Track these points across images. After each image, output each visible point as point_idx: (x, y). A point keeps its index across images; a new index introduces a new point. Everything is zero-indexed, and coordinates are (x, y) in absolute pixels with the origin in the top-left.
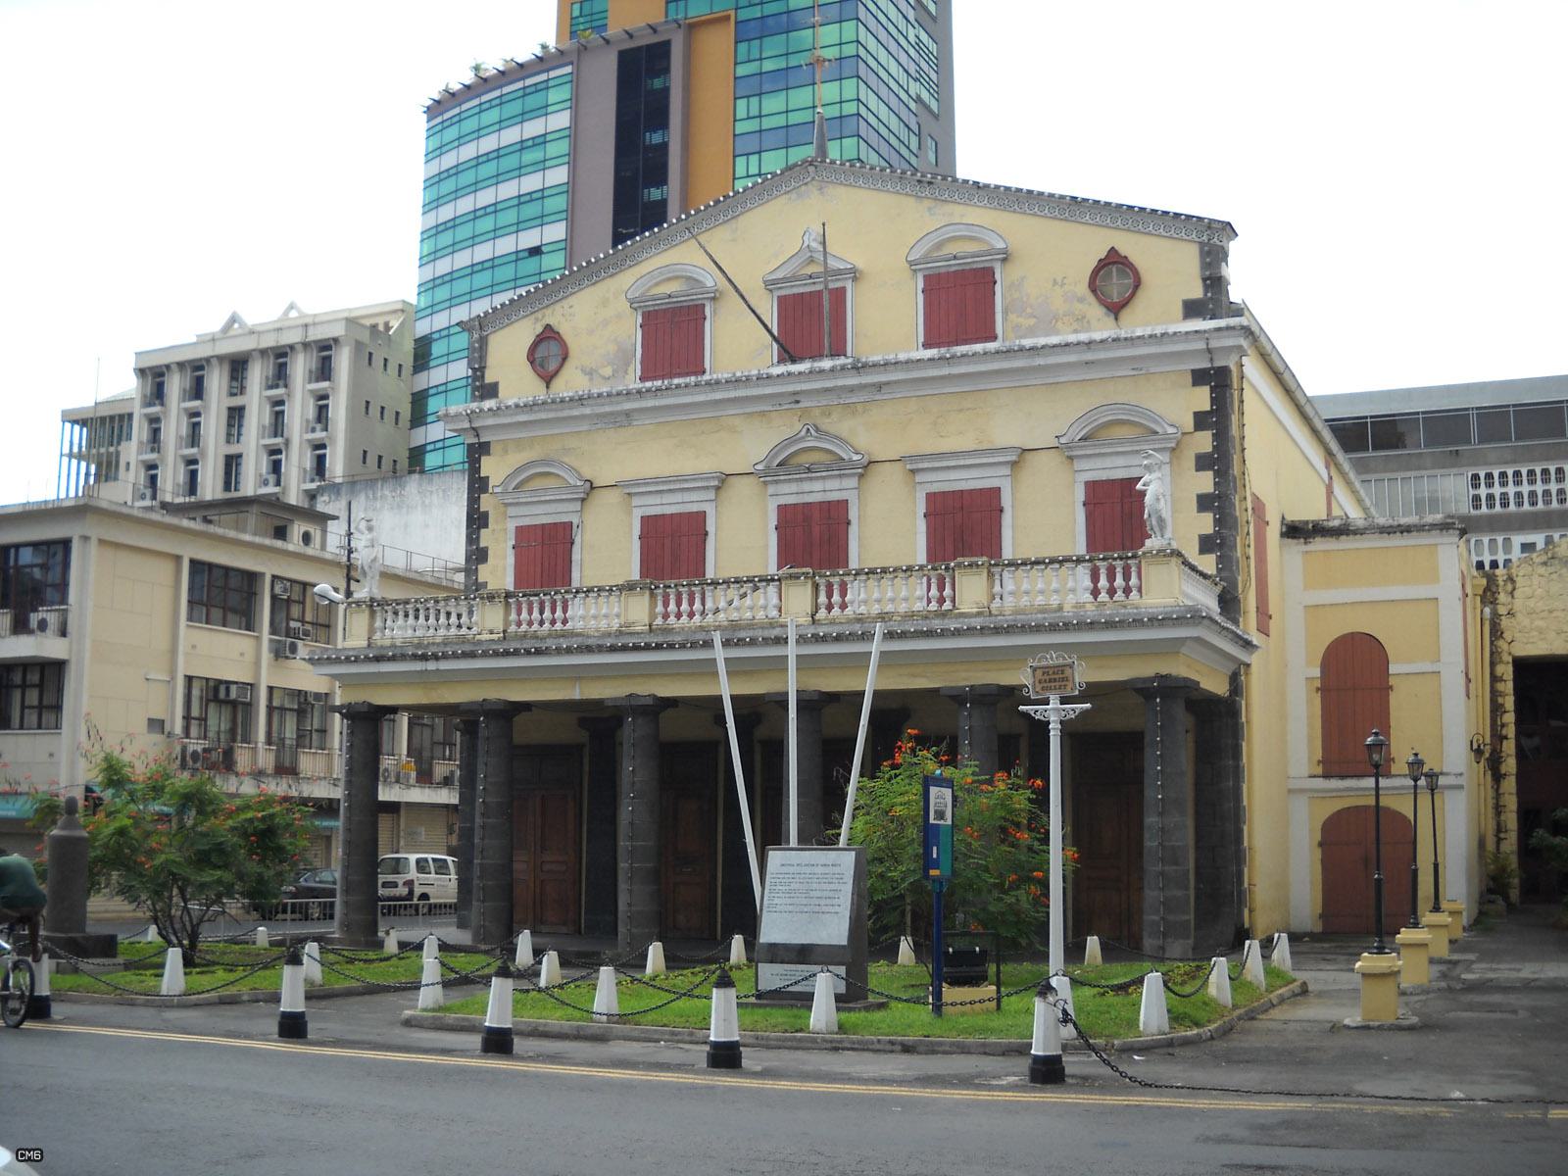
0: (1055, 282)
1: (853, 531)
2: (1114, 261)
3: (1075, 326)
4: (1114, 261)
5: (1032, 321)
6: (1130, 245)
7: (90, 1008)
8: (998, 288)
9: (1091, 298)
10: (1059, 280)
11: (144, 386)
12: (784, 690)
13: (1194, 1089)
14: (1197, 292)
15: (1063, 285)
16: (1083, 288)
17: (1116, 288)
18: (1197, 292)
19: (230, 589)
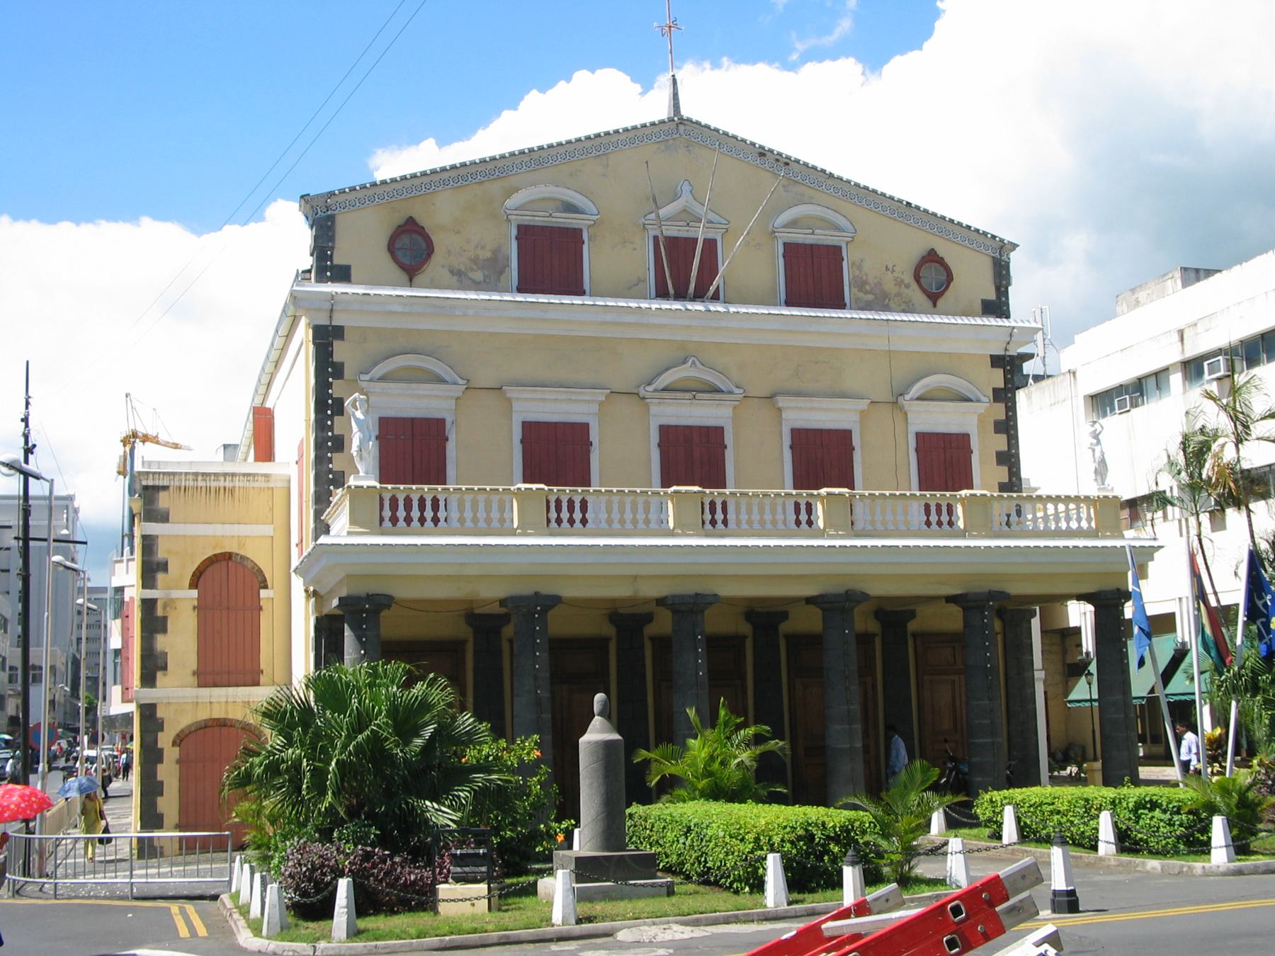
0: (887, 268)
1: (729, 454)
2: (932, 257)
3: (903, 307)
4: (932, 257)
5: (870, 297)
6: (944, 250)
7: (459, 886)
8: (845, 264)
9: (914, 285)
10: (890, 267)
11: (492, 602)
12: (353, 277)
13: (800, 409)
14: (992, 296)
15: (893, 271)
16: (908, 278)
17: (932, 275)
18: (992, 296)
19: (51, 492)
